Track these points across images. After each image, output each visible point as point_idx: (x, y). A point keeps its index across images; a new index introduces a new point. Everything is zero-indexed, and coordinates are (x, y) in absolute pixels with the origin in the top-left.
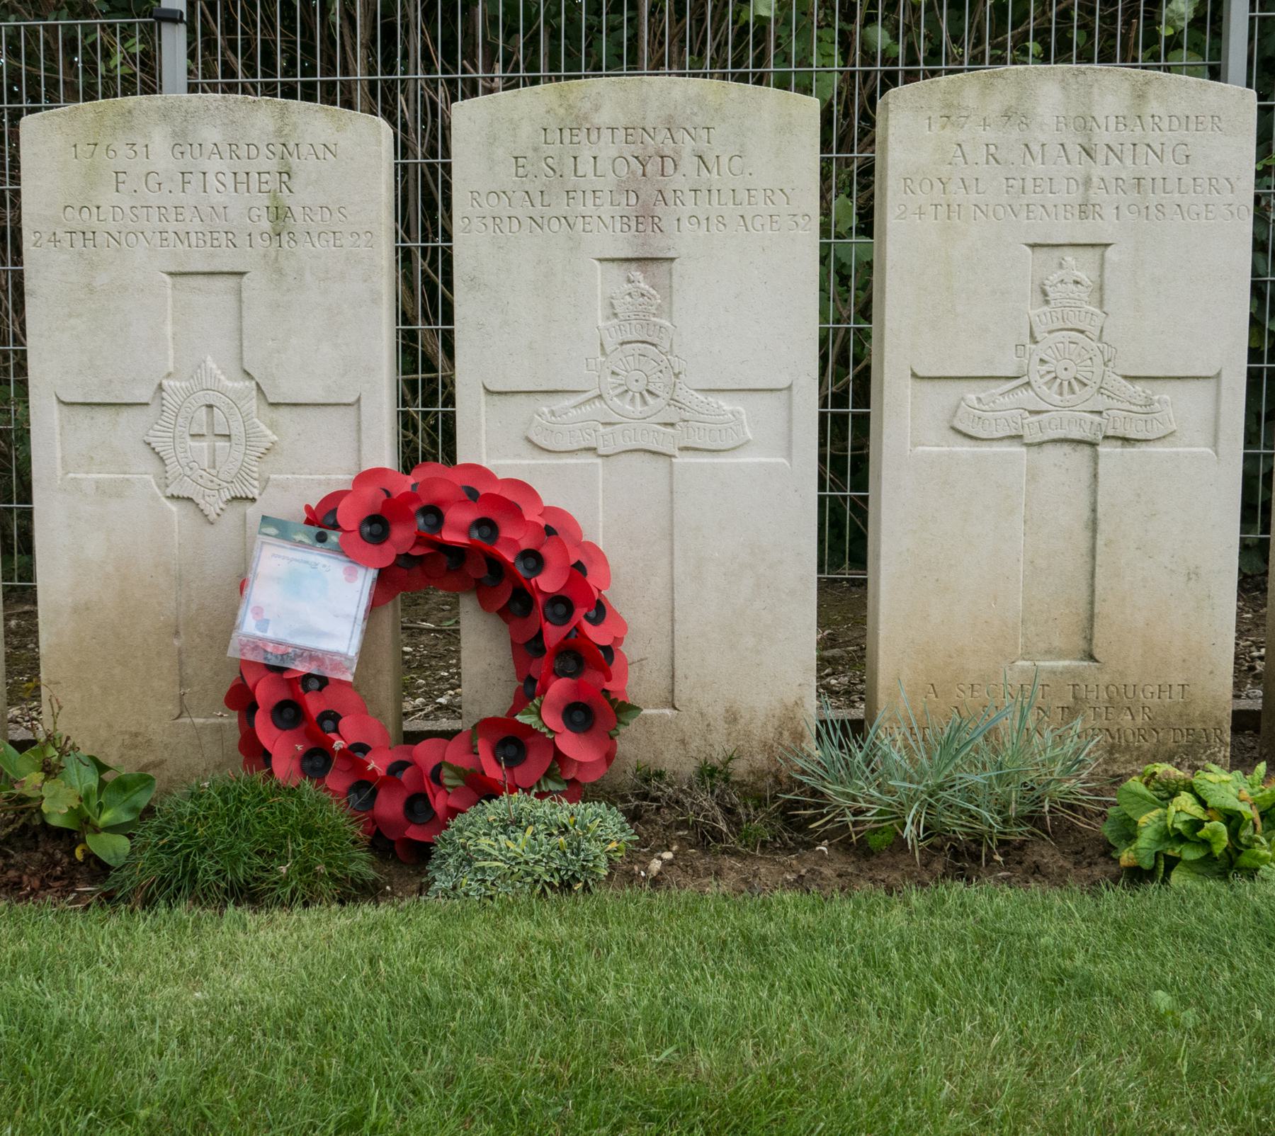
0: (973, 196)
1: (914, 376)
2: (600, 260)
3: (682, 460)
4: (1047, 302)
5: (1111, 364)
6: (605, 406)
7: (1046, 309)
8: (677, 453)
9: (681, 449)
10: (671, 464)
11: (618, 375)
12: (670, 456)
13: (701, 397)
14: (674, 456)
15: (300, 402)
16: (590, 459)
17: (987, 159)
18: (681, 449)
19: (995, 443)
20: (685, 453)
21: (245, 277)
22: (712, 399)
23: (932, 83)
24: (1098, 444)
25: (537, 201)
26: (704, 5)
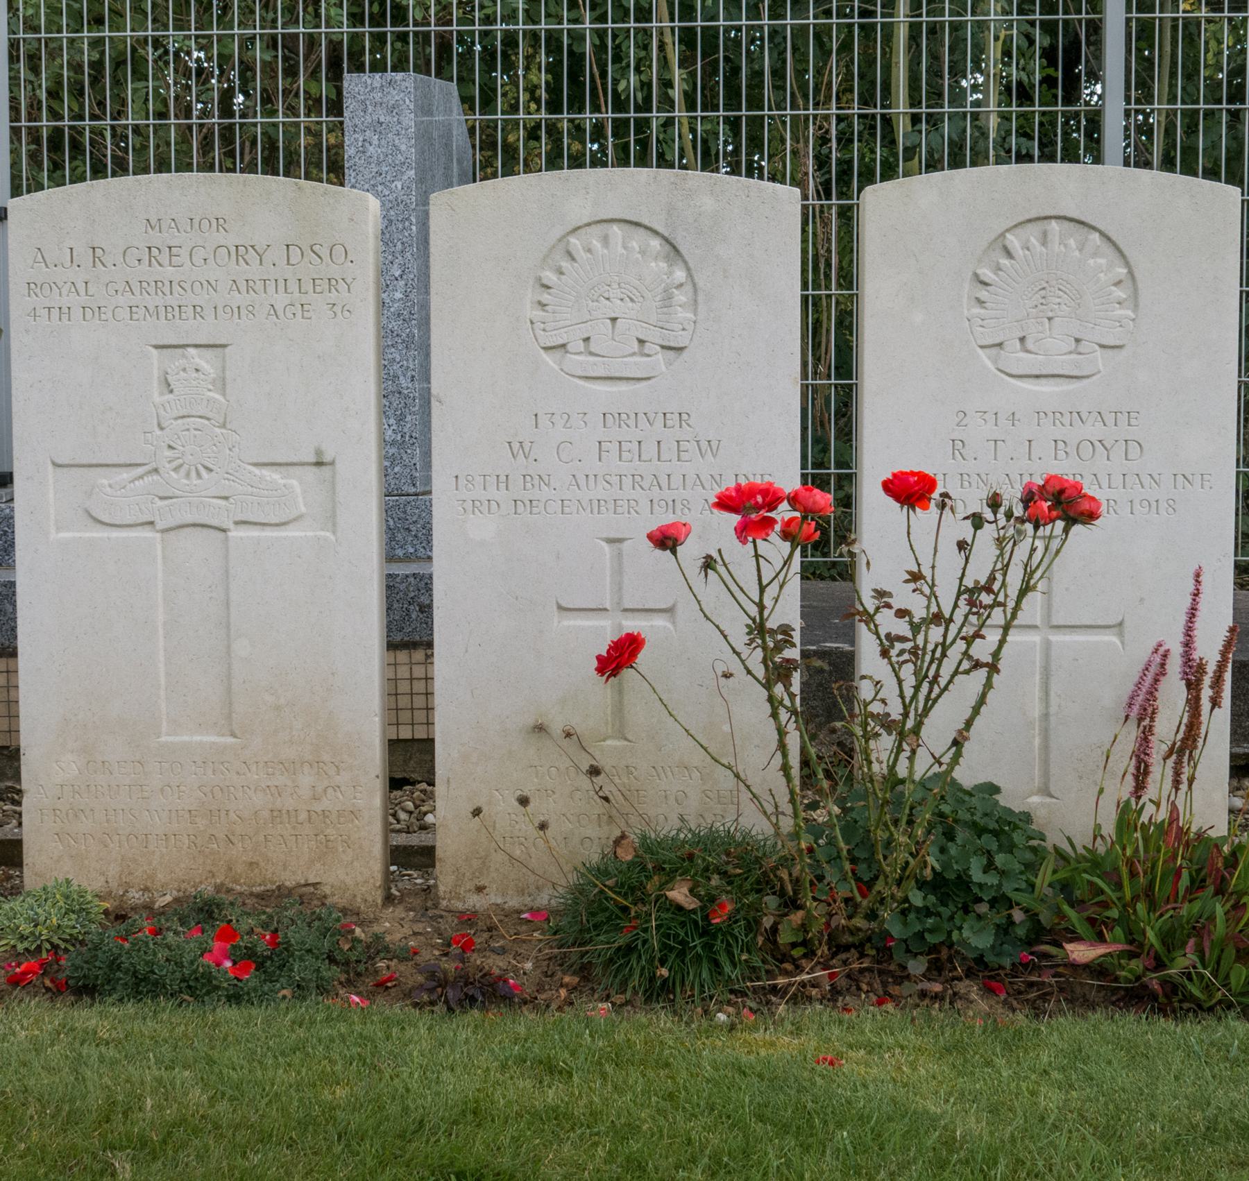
0: (83, 300)
1: (55, 465)
2: (156, 347)
3: (236, 533)
4: (171, 391)
5: (236, 450)
6: (161, 480)
7: (171, 396)
8: (232, 526)
9: (237, 523)
10: (227, 539)
11: (174, 448)
12: (224, 531)
13: (256, 470)
14: (229, 530)
15: (300, 468)
16: (147, 533)
17: (94, 261)
18: (237, 523)
19: (268, 528)
20: (239, 527)
21: (227, 350)
22: (266, 472)
23: (205, 177)
24: (229, 530)
25: (137, 290)
26: (673, 4)
